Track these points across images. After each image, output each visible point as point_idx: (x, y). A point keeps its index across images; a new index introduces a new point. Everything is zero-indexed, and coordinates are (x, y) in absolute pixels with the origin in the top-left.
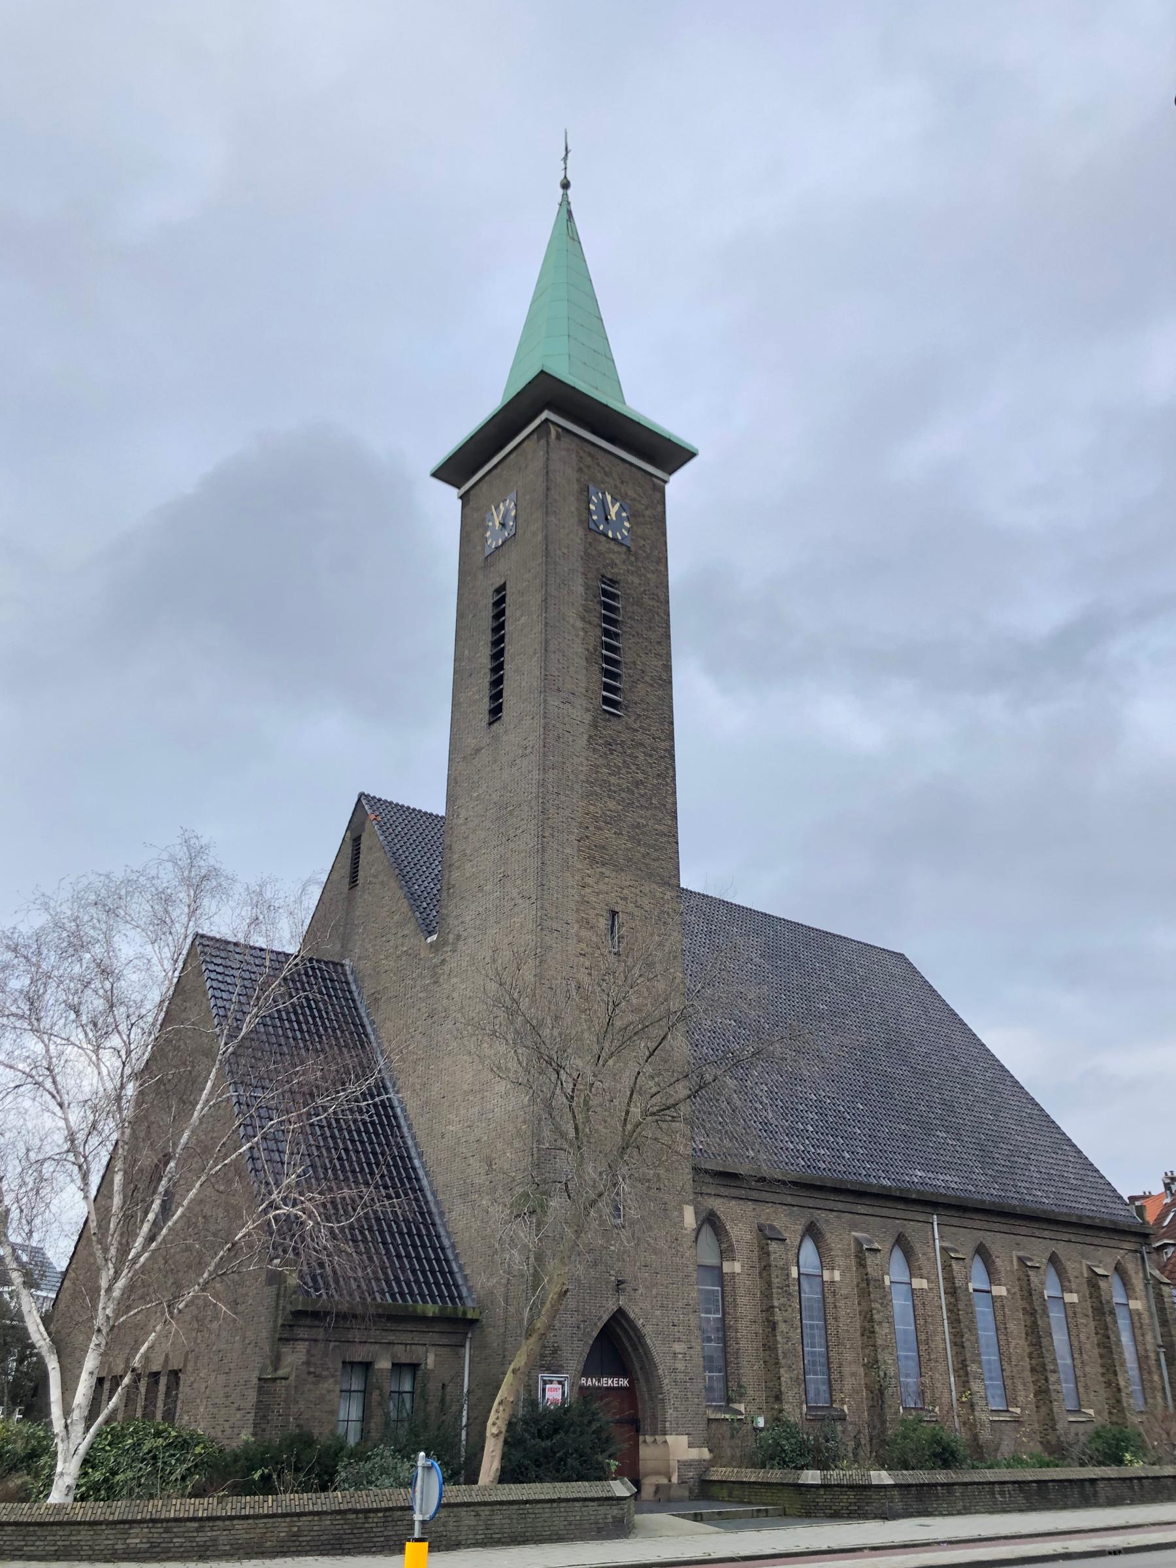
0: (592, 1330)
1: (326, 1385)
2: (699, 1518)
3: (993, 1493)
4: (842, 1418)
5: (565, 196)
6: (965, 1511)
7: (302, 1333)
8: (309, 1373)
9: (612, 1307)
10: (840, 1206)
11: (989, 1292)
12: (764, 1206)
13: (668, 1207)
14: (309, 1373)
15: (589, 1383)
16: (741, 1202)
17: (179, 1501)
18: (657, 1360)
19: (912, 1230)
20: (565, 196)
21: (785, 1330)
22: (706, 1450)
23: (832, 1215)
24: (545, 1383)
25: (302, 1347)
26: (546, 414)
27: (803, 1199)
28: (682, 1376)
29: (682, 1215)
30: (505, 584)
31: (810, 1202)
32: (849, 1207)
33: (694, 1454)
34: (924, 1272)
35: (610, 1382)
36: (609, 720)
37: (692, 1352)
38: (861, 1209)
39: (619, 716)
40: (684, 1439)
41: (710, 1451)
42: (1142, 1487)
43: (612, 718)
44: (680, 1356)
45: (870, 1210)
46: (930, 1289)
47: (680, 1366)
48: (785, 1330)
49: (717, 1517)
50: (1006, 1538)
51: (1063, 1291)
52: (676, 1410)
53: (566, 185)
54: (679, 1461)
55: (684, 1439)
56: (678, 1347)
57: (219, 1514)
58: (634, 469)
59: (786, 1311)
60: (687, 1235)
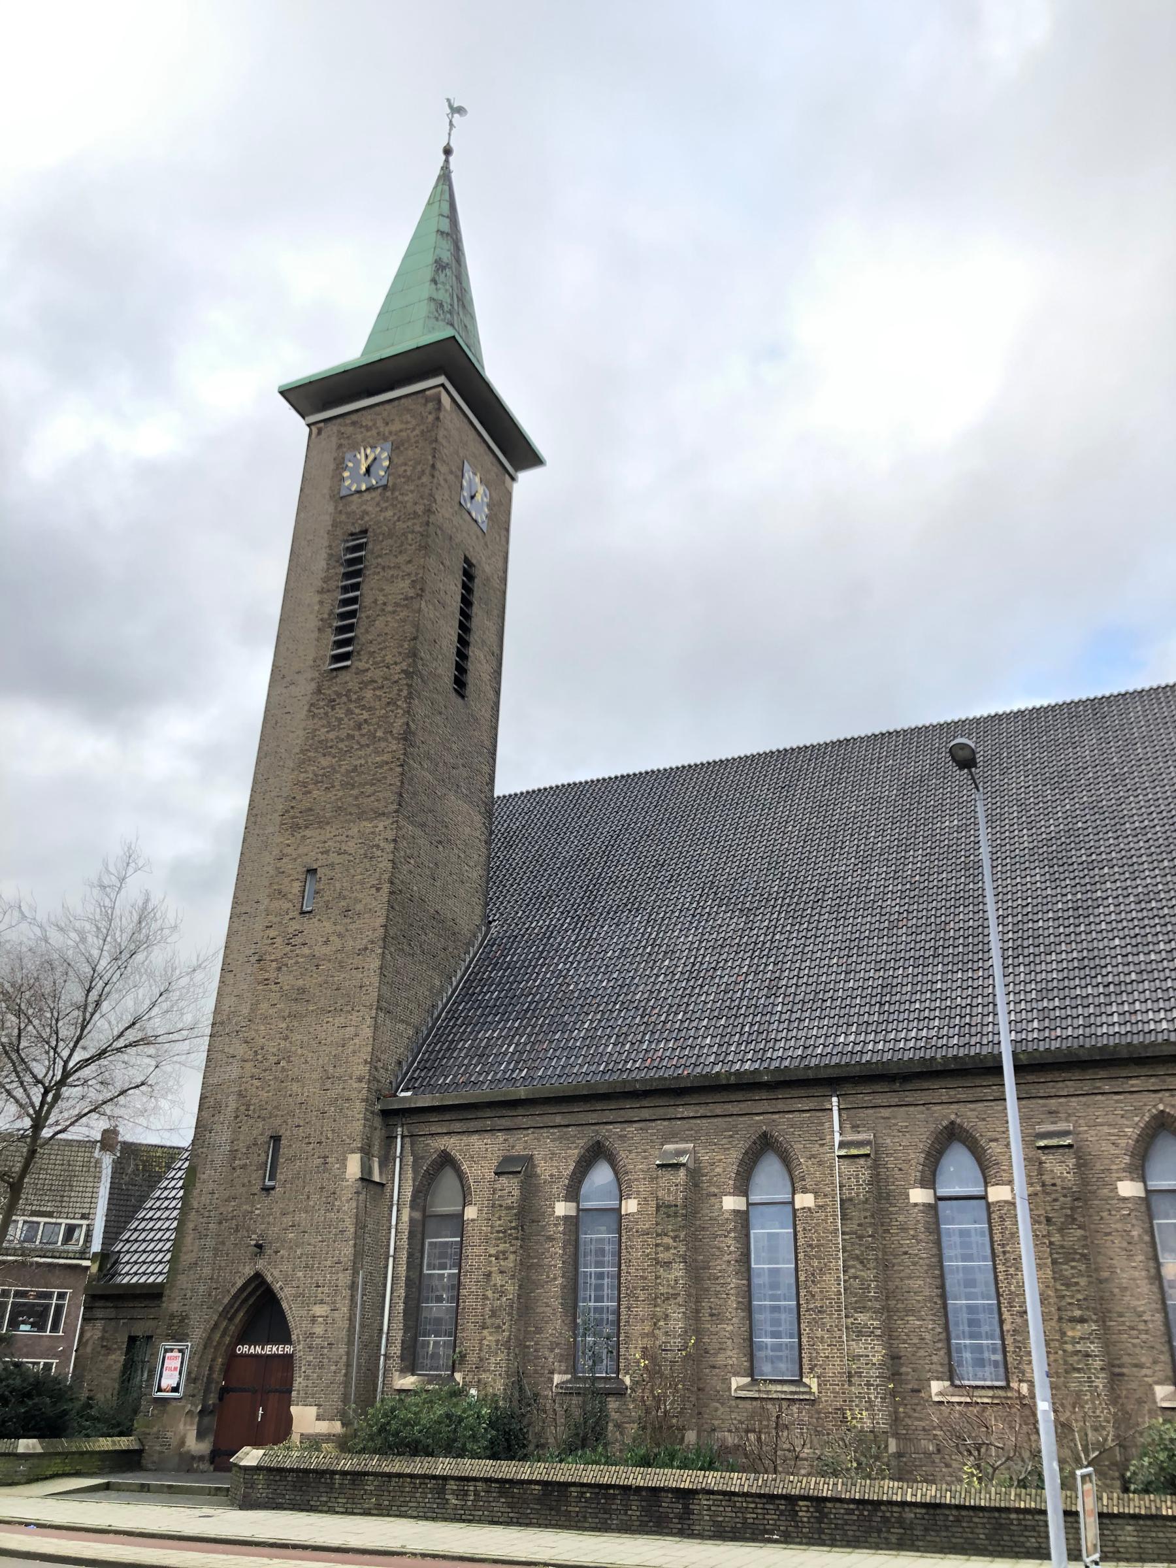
0: (224, 1297)
1: (113, 1357)
2: (146, 1489)
3: (441, 1492)
4: (620, 1393)
5: (447, 161)
6: (381, 1511)
7: (99, 1313)
8: (103, 1346)
9: (248, 1271)
10: (645, 1114)
11: (984, 1197)
12: (520, 1135)
13: (329, 1160)
14: (103, 1346)
15: (252, 1351)
16: (487, 1135)
17: (814, 1479)
18: (292, 1324)
19: (968, 1116)
20: (447, 161)
21: (499, 1283)
22: (339, 1423)
23: (631, 1128)
24: (166, 1351)
25: (99, 1325)
26: (442, 379)
27: (581, 1115)
28: (319, 1341)
29: (344, 1166)
30: (467, 560)
31: (592, 1118)
32: (660, 1112)
33: (323, 1427)
34: (809, 1182)
35: (274, 1349)
36: (337, 676)
37: (336, 1314)
38: (681, 1111)
39: (346, 667)
40: (313, 1410)
41: (343, 1425)
42: (822, 1516)
43: (339, 673)
44: (320, 1319)
45: (702, 1111)
46: (820, 1207)
47: (319, 1330)
48: (499, 1283)
49: (166, 1490)
50: (305, 1547)
51: (986, 1184)
52: (307, 1378)
53: (448, 151)
54: (302, 1435)
55: (313, 1410)
56: (319, 1310)
57: (997, 1505)
58: (396, 403)
59: (507, 1259)
60: (347, 1187)
